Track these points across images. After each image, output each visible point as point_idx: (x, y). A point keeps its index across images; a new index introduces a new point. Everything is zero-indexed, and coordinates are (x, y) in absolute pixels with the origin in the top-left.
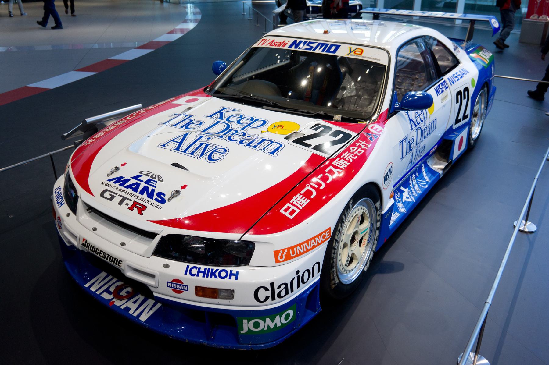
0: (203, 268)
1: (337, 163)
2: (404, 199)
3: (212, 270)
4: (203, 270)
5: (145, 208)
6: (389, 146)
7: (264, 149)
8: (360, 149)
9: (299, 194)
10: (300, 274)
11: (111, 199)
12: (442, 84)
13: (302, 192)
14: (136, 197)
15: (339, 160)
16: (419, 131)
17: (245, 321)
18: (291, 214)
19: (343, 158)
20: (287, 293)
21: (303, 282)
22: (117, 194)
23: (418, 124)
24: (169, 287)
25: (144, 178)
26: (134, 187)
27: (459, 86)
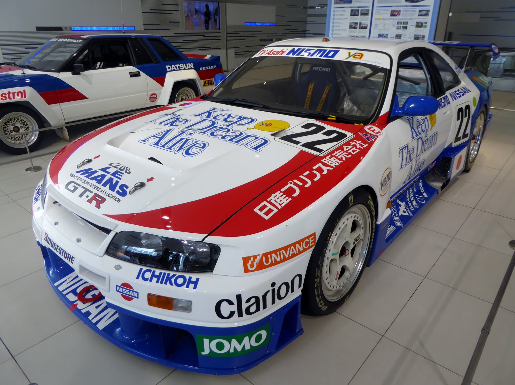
0: (157, 272)
1: (328, 161)
2: (401, 213)
3: (169, 274)
4: (158, 274)
5: (104, 200)
6: (388, 155)
7: (247, 144)
8: (354, 149)
9: (279, 192)
10: (276, 287)
11: (73, 191)
12: (444, 98)
13: (283, 190)
14: (98, 189)
15: (330, 158)
16: (420, 142)
17: (206, 341)
18: (267, 214)
19: (334, 156)
20: (258, 309)
21: (280, 298)
22: (80, 185)
23: (420, 134)
24: (118, 291)
25: (112, 170)
26: (99, 179)
27: (462, 102)
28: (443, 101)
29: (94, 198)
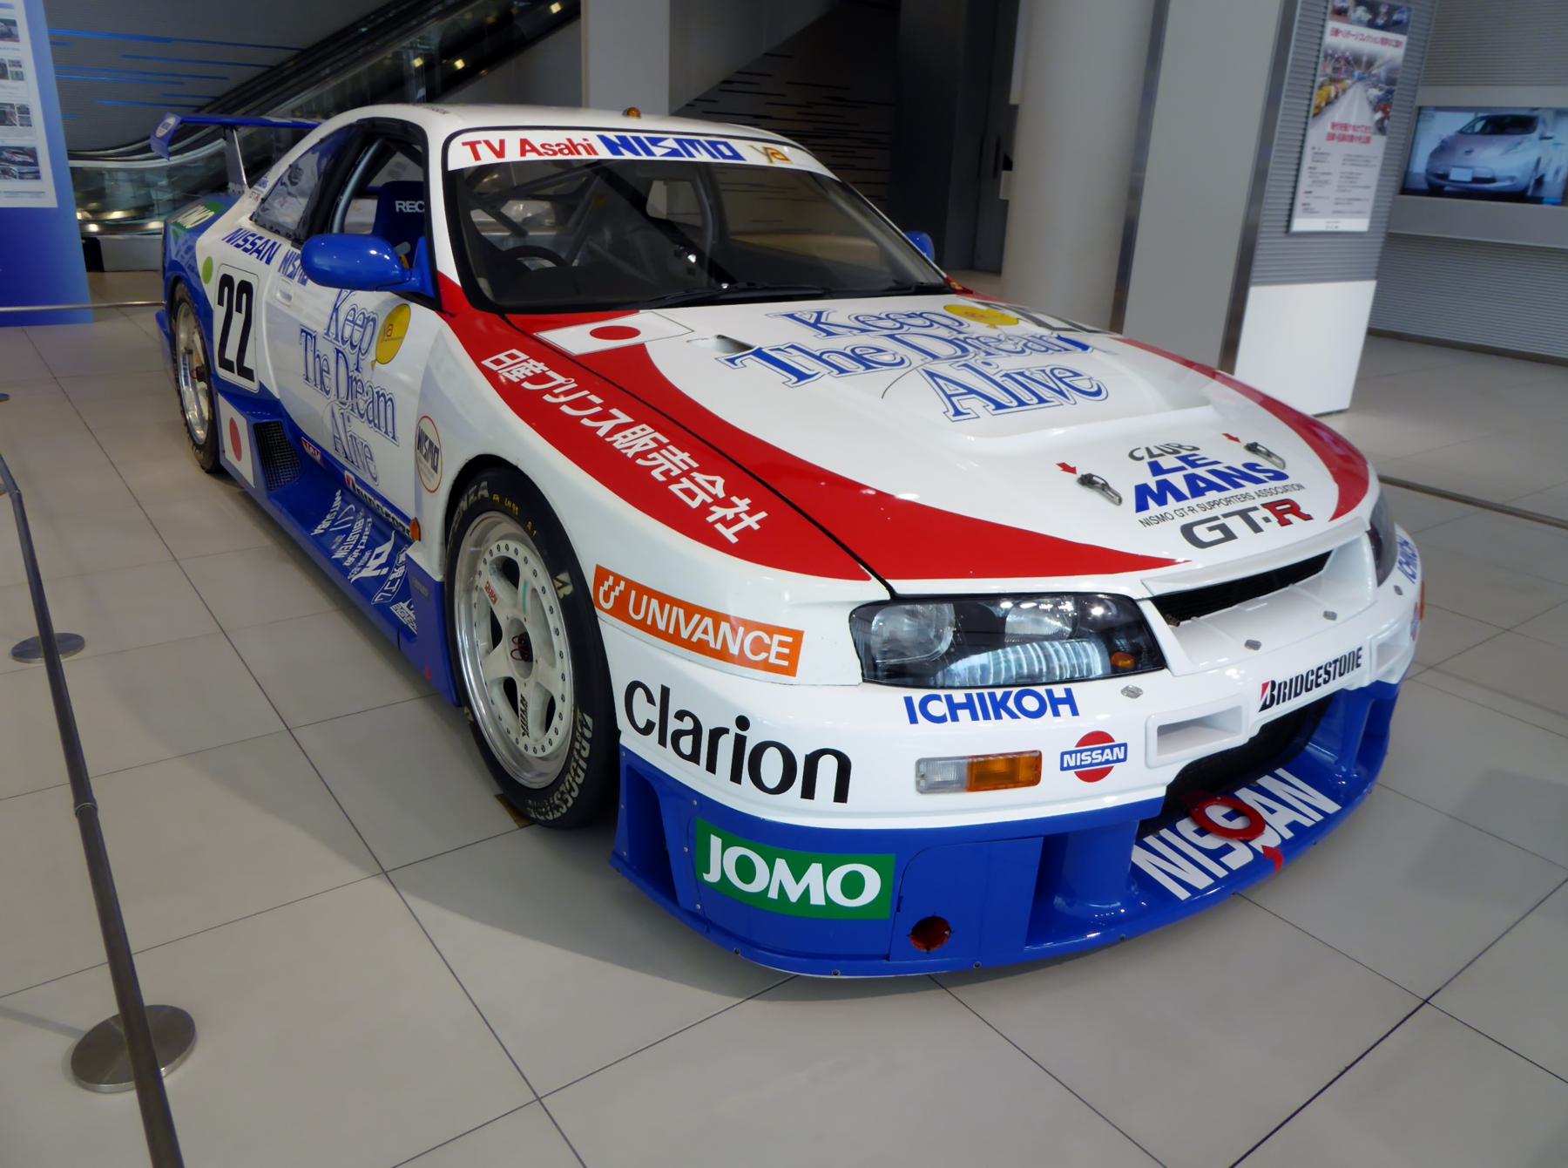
3: (992, 696)
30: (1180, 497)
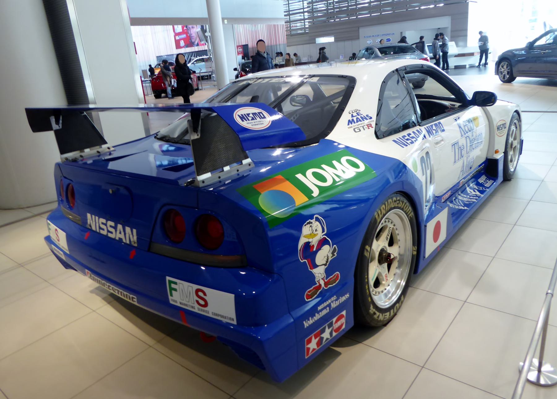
28: (434, 128)
29: (368, 127)
30: (354, 123)
